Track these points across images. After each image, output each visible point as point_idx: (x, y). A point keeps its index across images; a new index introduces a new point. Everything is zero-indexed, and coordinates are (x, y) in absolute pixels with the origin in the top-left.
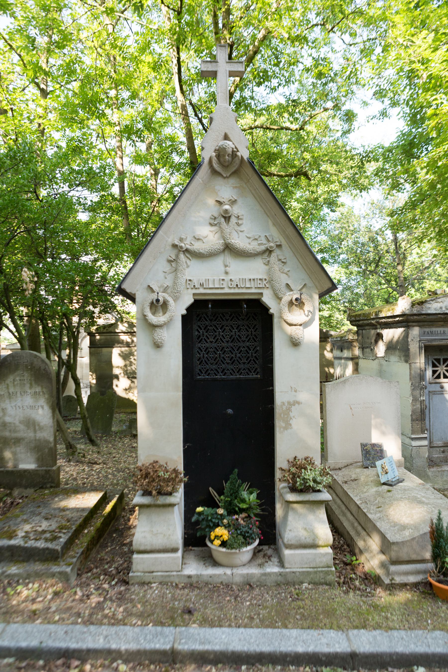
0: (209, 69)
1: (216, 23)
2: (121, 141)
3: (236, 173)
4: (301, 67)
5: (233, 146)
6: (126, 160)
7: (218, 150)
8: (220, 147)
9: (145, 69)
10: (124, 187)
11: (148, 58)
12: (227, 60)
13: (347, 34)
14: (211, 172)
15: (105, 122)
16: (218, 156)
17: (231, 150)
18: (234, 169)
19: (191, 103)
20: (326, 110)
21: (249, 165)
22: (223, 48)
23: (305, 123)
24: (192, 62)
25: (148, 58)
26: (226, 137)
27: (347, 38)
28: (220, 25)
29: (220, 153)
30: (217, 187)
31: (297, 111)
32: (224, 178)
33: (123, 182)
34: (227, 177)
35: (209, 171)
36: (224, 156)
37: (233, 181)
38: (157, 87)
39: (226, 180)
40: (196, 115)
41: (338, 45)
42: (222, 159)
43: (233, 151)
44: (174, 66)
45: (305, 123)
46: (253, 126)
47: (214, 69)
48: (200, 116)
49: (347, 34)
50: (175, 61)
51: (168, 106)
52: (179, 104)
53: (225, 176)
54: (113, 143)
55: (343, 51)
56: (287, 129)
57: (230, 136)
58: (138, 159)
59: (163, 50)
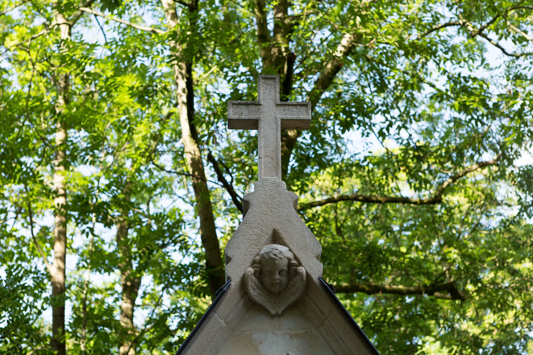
0: (243, 117)
1: (262, 24)
2: (64, 224)
3: (296, 307)
4: (428, 90)
5: (290, 255)
6: (72, 259)
7: (259, 262)
8: (263, 257)
9: (123, 97)
10: (62, 316)
11: (130, 80)
12: (279, 102)
13: (510, 39)
14: (245, 304)
15: (37, 188)
16: (260, 274)
17: (286, 261)
18: (293, 299)
19: (210, 158)
20: (483, 165)
21: (322, 291)
22: (271, 82)
23: (442, 191)
24: (216, 85)
25: (130, 80)
26: (276, 238)
27: (508, 45)
28: (271, 26)
29: (264, 267)
30: (257, 336)
31: (425, 166)
32: (272, 317)
33: (63, 309)
34: (278, 316)
35: (241, 303)
36: (272, 273)
37: (288, 323)
38: (142, 130)
39: (276, 320)
40: (221, 178)
41: (493, 55)
42: (266, 280)
43: (290, 265)
44: (180, 91)
45: (442, 191)
46: (336, 196)
47: (252, 117)
48: (228, 178)
49: (510, 39)
50: (182, 84)
51: (166, 160)
52: (188, 157)
53: (273, 312)
54: (48, 219)
55: (504, 67)
56: (405, 201)
57: (284, 235)
58: (97, 260)
59: (160, 64)
